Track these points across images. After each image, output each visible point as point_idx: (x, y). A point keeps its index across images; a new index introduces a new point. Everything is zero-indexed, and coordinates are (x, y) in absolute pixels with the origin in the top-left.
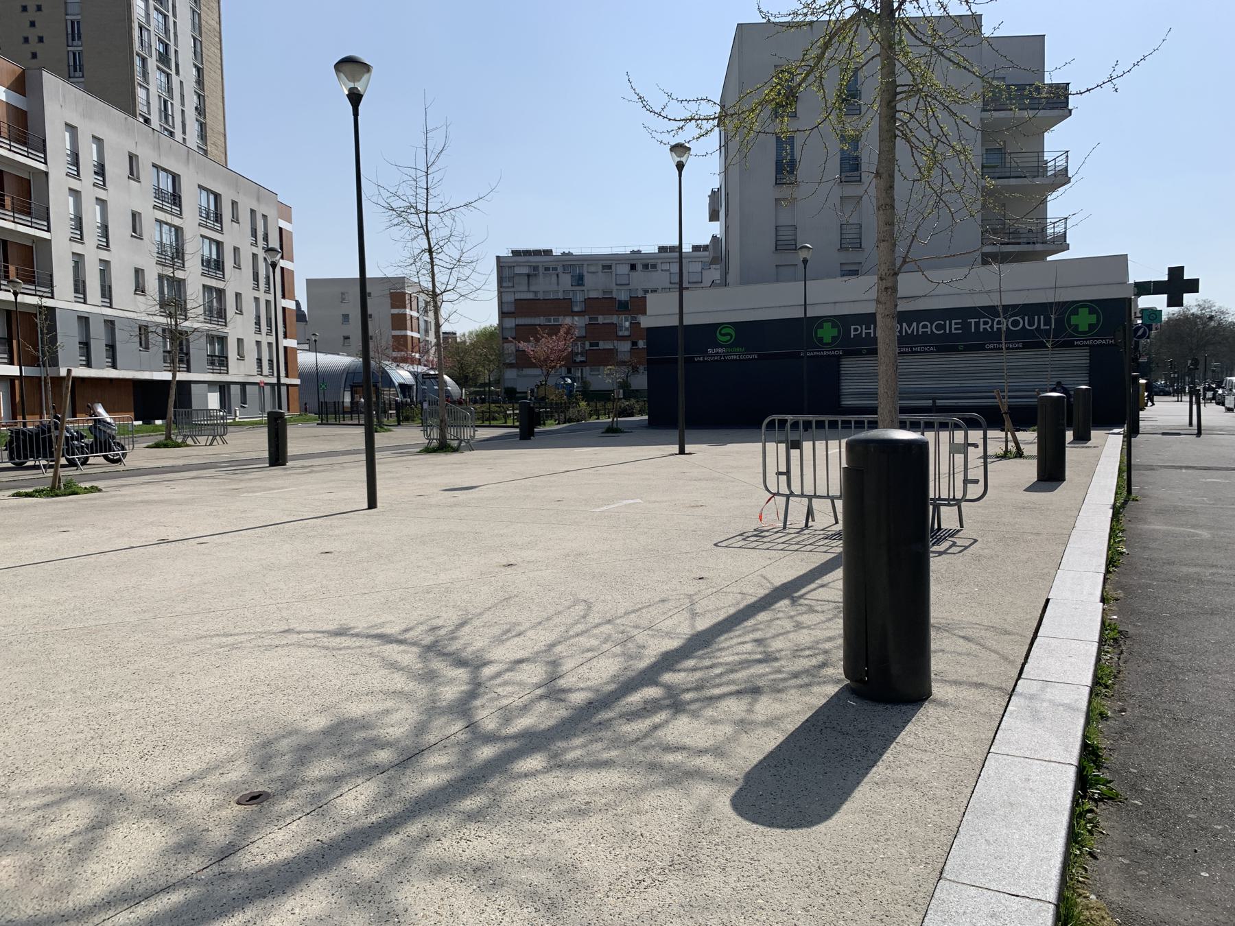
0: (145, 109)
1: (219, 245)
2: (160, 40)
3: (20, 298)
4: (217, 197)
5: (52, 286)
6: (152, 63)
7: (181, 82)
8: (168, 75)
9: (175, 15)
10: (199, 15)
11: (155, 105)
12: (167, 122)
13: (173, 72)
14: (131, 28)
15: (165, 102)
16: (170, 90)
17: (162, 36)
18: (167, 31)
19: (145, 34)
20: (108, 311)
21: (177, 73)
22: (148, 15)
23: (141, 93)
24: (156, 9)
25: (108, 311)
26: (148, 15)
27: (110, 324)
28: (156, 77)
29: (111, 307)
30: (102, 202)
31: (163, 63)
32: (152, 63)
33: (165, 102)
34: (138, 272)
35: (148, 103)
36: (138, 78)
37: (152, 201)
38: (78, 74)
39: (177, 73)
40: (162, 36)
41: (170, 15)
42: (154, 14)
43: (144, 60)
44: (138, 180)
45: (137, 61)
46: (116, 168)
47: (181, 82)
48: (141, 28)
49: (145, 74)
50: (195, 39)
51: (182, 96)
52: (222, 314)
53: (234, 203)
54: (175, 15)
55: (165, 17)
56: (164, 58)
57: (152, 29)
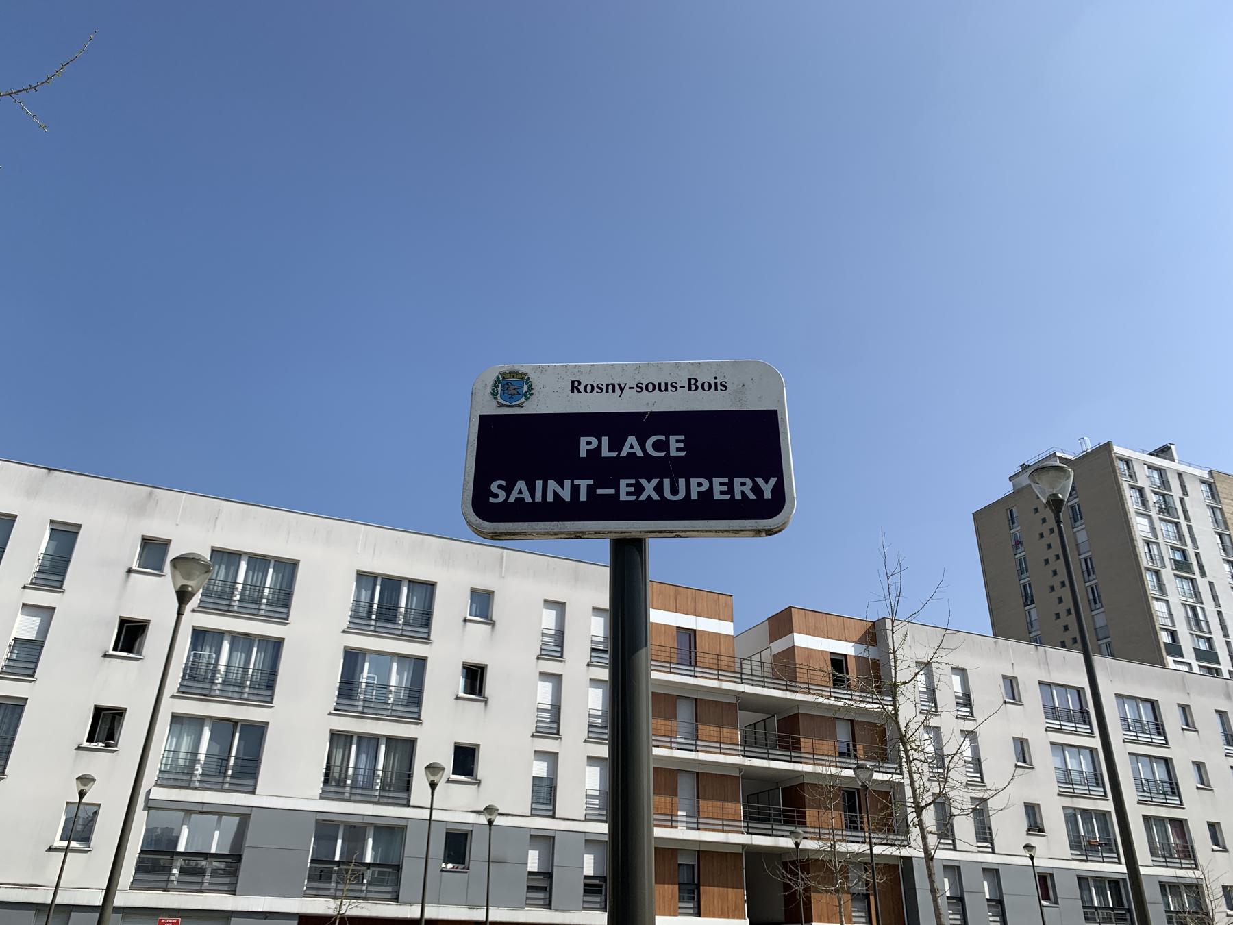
0: (1168, 622)
1: (1167, 762)
2: (1172, 548)
3: (877, 850)
4: (1153, 704)
5: (992, 839)
6: (1168, 574)
7: (1211, 584)
8: (1192, 580)
9: (1187, 518)
10: (1221, 509)
11: (1179, 614)
12: (1200, 629)
13: (1197, 576)
14: (1134, 547)
15: (1194, 609)
16: (1197, 594)
17: (1176, 543)
18: (1181, 537)
19: (1154, 548)
20: (990, 858)
21: (1203, 574)
22: (1153, 529)
23: (1159, 608)
24: (1162, 520)
25: (990, 858)
26: (1153, 529)
27: (992, 873)
28: (1176, 589)
29: (993, 852)
30: (971, 735)
31: (1181, 570)
32: (1168, 574)
33: (1194, 609)
34: (1032, 810)
35: (1171, 615)
36: (1152, 590)
37: (1043, 722)
38: (1098, 605)
39: (1203, 574)
40: (1176, 543)
41: (1182, 520)
42: (1160, 526)
43: (1157, 573)
44: (1020, 703)
45: (1149, 579)
46: (987, 694)
47: (1211, 584)
48: (1148, 543)
49: (1161, 586)
50: (1220, 535)
51: (1215, 597)
52: (1187, 853)
53: (1185, 709)
54: (1187, 518)
55: (1177, 524)
56: (1182, 565)
57: (1160, 540)
